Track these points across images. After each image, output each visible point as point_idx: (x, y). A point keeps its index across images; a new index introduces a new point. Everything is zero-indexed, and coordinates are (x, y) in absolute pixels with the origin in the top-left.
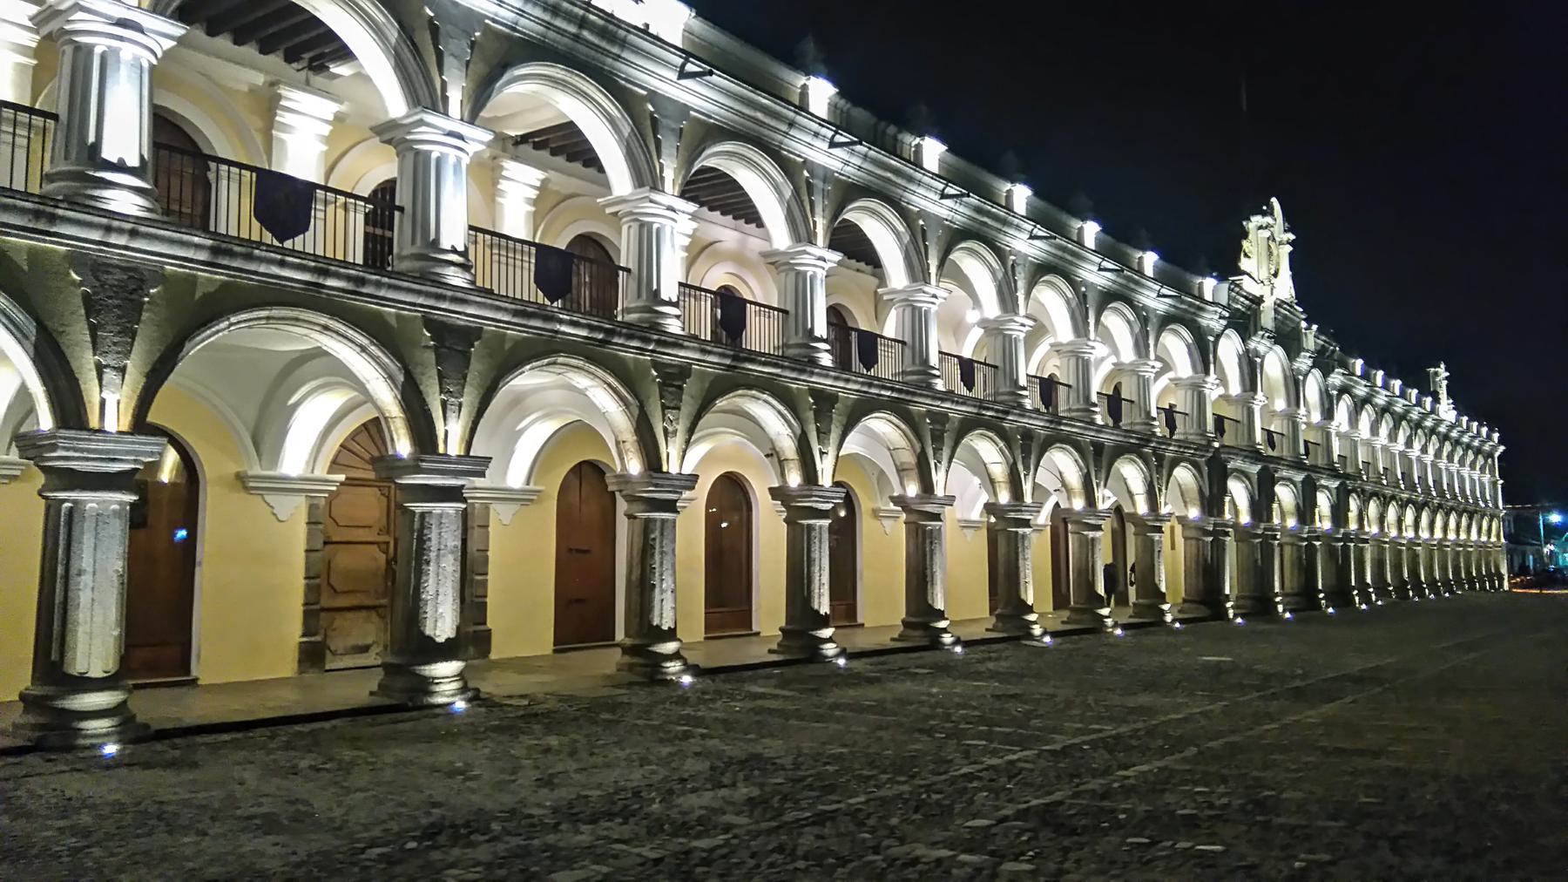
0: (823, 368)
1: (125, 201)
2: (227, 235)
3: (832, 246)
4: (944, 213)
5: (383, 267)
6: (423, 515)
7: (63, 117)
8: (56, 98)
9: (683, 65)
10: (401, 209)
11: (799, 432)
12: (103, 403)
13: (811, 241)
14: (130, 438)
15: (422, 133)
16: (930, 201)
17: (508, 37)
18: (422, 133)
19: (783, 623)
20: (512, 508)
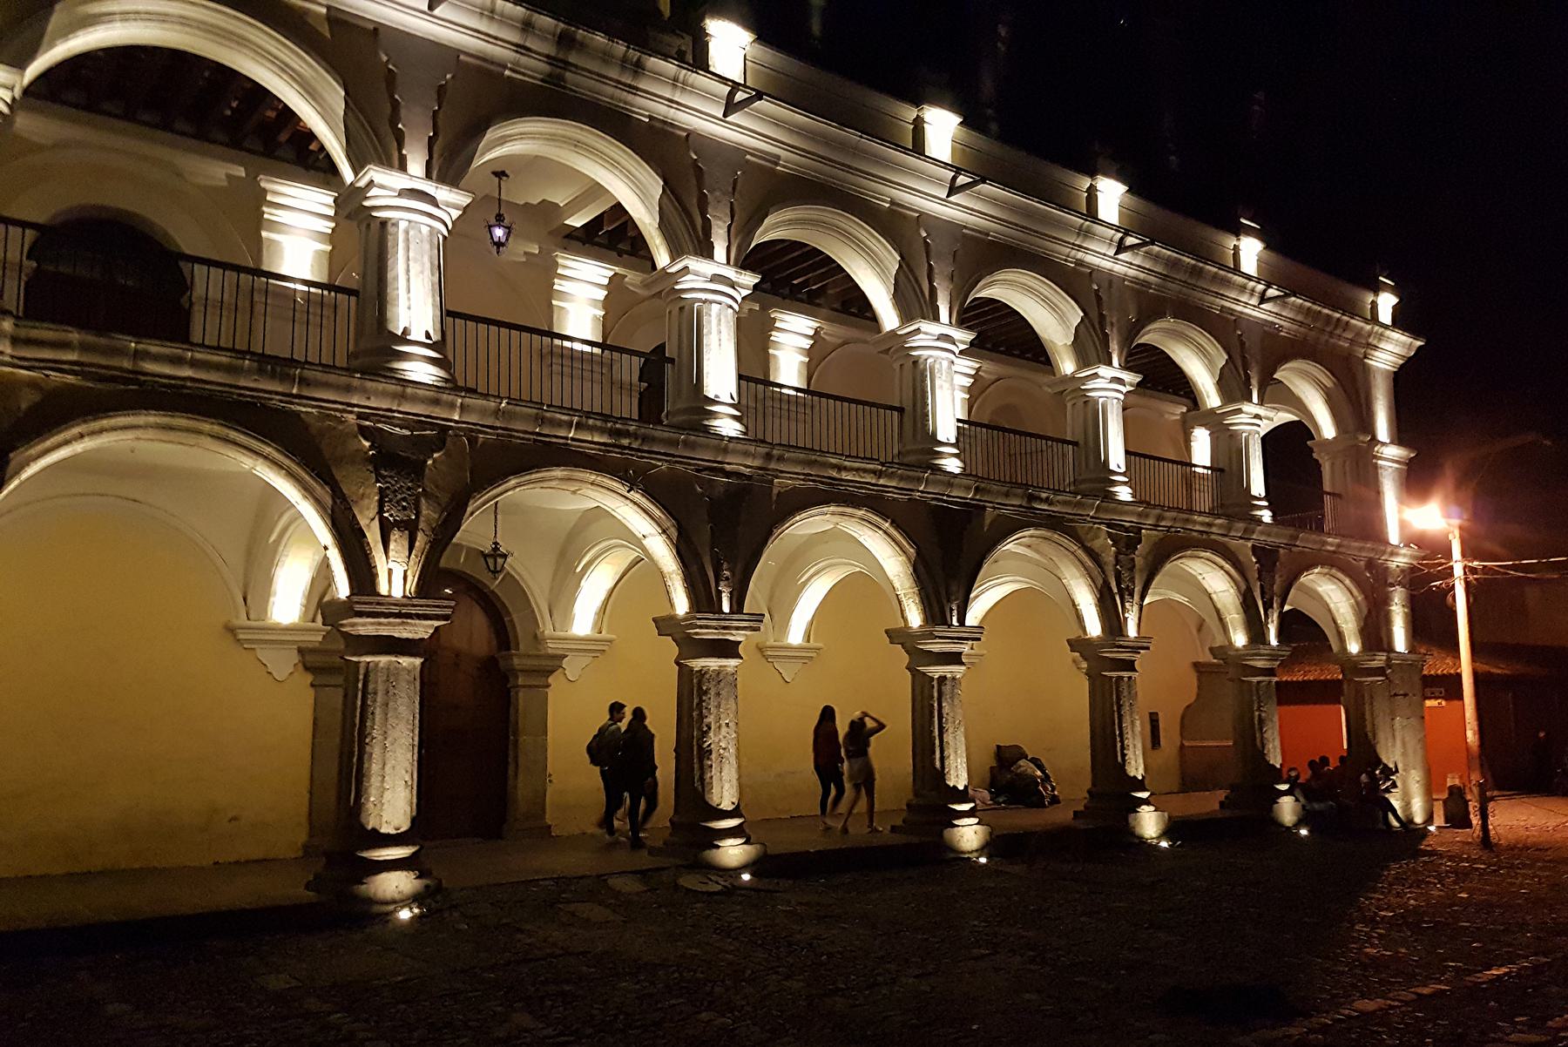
0: (1121, 502)
1: (421, 372)
2: (263, 355)
3: (1126, 367)
4: (1119, 269)
5: (640, 414)
6: (942, 679)
7: (1081, 443)
8: (353, 278)
9: (954, 179)
10: (672, 361)
11: (1244, 587)
12: (390, 571)
13: (706, 252)
14: (415, 602)
15: (687, 282)
16: (1256, 307)
17: (479, 69)
18: (687, 282)
19: (1088, 785)
20: (585, 660)
